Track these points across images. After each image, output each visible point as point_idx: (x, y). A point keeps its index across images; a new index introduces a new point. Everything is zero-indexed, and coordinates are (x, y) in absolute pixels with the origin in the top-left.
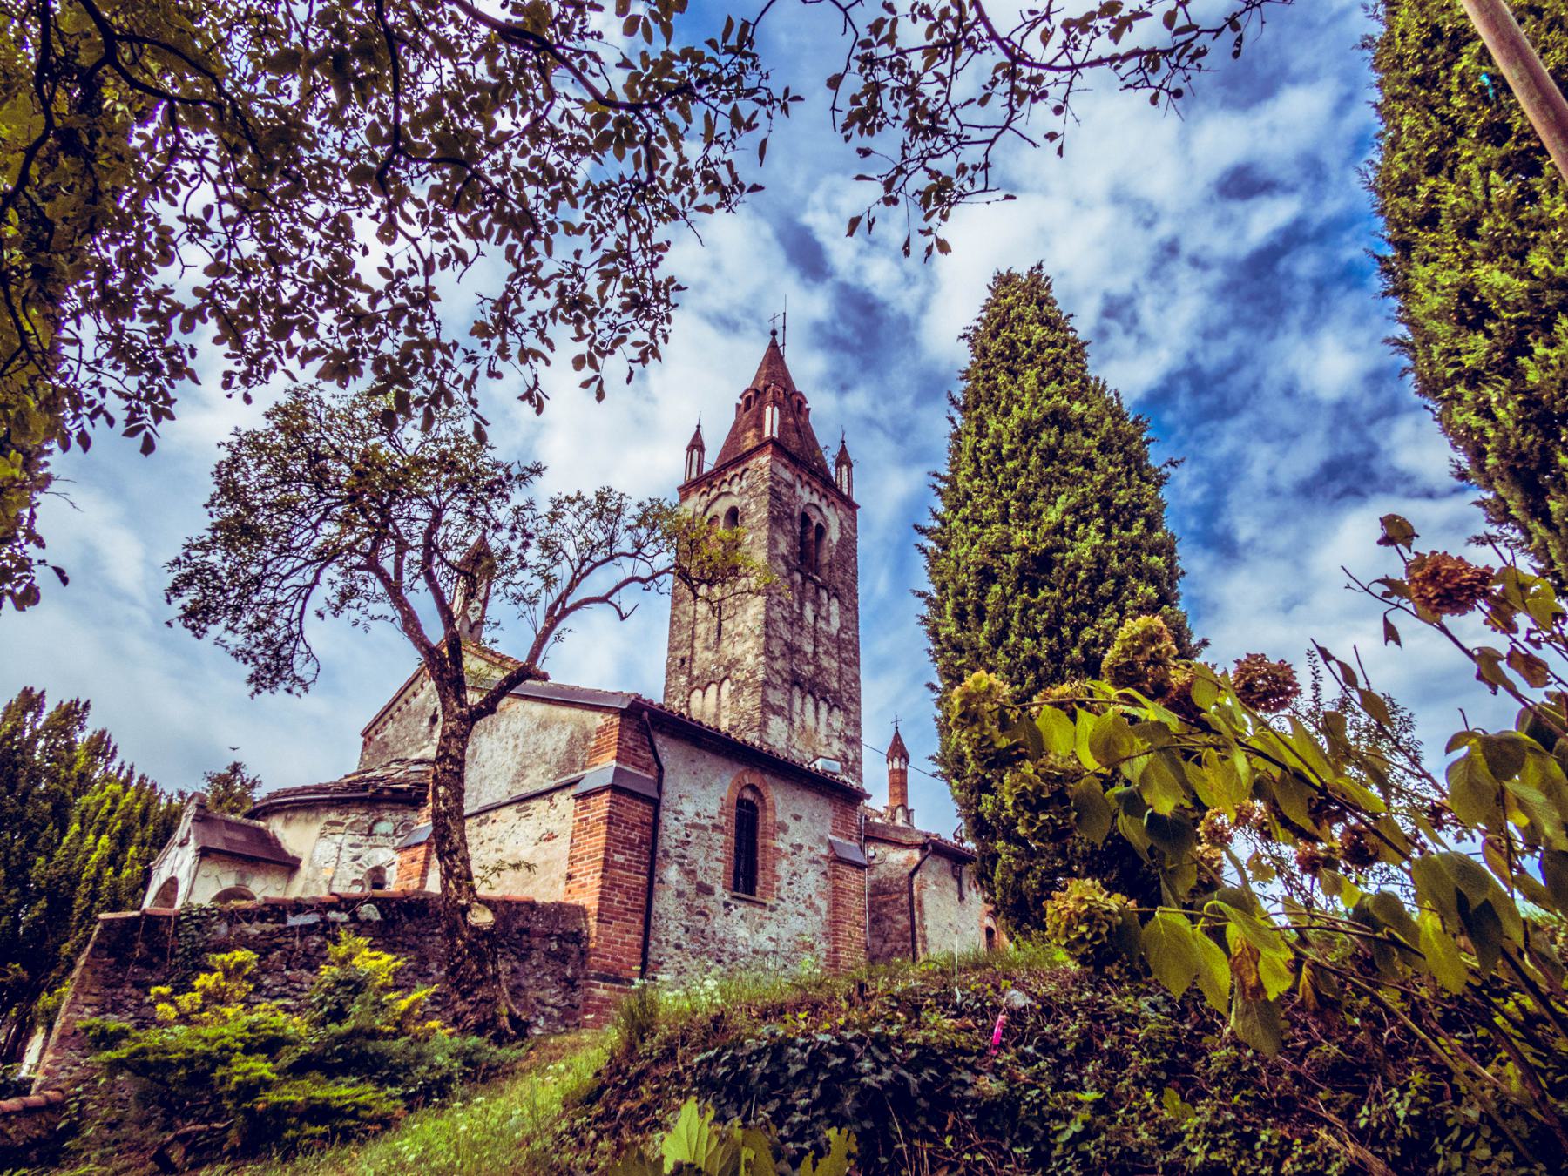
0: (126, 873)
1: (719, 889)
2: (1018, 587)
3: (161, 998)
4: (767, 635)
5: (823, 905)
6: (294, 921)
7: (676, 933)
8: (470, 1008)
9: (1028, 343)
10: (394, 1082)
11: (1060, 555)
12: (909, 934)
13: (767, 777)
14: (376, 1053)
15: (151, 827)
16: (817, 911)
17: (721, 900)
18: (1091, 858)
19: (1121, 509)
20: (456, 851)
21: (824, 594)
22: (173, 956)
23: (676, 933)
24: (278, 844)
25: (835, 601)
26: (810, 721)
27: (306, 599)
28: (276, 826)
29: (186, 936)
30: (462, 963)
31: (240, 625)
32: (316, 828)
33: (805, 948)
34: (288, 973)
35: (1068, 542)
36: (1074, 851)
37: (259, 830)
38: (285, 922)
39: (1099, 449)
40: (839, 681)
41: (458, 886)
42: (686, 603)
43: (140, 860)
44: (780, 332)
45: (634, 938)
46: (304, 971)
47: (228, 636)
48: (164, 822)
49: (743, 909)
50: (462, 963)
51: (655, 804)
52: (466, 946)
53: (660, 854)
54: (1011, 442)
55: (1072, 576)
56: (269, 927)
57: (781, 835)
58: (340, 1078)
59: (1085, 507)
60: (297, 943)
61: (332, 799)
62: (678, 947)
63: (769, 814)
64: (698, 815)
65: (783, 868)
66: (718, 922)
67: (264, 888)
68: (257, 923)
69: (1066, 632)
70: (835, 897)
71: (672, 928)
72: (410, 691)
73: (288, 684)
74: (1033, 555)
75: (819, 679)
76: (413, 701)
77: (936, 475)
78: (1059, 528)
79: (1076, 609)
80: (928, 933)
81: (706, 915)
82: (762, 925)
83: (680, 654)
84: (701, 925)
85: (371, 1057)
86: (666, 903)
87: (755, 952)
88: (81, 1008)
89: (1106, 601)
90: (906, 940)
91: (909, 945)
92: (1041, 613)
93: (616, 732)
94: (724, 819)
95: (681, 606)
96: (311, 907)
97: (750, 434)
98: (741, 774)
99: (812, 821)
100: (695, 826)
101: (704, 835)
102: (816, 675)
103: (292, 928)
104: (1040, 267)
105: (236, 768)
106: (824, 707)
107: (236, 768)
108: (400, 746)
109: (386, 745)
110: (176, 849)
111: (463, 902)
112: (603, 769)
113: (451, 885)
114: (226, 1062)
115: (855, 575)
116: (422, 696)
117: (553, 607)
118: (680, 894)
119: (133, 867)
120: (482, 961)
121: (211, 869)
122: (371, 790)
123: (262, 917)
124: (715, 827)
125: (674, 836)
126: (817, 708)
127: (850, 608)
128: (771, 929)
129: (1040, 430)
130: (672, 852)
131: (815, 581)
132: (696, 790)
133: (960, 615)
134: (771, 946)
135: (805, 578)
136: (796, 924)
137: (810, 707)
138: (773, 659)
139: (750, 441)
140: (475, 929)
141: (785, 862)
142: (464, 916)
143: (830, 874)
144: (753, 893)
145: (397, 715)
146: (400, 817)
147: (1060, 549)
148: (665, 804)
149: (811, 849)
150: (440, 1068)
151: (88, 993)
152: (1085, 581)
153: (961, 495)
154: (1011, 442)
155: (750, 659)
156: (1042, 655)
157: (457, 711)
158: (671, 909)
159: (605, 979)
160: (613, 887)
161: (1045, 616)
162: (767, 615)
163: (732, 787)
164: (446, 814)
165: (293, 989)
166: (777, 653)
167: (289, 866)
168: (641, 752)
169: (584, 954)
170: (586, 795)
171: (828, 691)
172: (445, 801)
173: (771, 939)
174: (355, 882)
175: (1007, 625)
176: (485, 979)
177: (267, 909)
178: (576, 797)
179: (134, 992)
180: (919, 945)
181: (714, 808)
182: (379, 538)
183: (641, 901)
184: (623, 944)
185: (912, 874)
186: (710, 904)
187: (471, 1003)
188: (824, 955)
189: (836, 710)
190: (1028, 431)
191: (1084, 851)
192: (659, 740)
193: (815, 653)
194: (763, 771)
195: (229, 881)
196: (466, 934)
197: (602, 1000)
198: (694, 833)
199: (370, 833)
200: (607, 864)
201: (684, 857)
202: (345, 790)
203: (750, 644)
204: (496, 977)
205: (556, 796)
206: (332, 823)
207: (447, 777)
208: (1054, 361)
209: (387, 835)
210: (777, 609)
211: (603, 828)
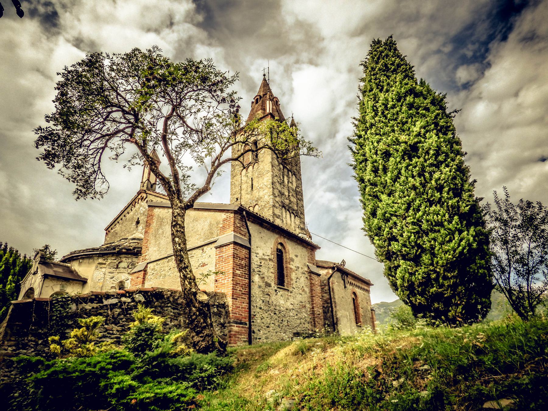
0: (8, 287)
1: (273, 284)
2: (403, 158)
3: (54, 341)
4: (273, 187)
5: (307, 290)
6: (106, 302)
7: (259, 303)
8: (201, 339)
9: (392, 64)
10: (185, 379)
11: (421, 145)
12: (329, 301)
13: (286, 240)
14: (173, 365)
15: (18, 268)
16: (306, 293)
17: (274, 289)
18: (446, 265)
19: (442, 127)
20: (187, 267)
21: (290, 173)
22: (51, 320)
23: (259, 303)
24: (77, 273)
25: (294, 176)
26: (289, 222)
27: (101, 154)
28: (75, 266)
29: (57, 311)
30: (196, 318)
31: (70, 165)
32: (93, 267)
33: (303, 307)
34: (106, 326)
35: (423, 140)
36: (437, 263)
37: (68, 267)
38: (102, 303)
39: (431, 103)
40: (297, 206)
41: (190, 283)
42: (237, 177)
43: (14, 282)
44: (267, 75)
45: (245, 305)
46: (113, 325)
47: (64, 169)
48: (23, 265)
49: (281, 292)
50: (196, 318)
51: (249, 249)
52: (197, 311)
53: (252, 270)
54: (393, 101)
55: (427, 153)
56: (95, 305)
57: (292, 263)
58: (160, 380)
59: (428, 126)
60: (109, 312)
61: (100, 254)
62: (260, 308)
63: (287, 254)
64: (264, 255)
65: (293, 276)
66: (273, 297)
67: (72, 291)
68: (89, 304)
69: (427, 175)
70: (311, 287)
71: (258, 301)
72: (126, 212)
73: (92, 195)
74: (410, 145)
75: (291, 205)
76: (128, 216)
77: (354, 118)
78: (419, 134)
79: (431, 165)
80: (336, 300)
81: (269, 295)
82: (288, 299)
83: (236, 196)
84: (268, 299)
85: (171, 367)
86: (255, 290)
87: (287, 309)
88: (6, 347)
89: (442, 163)
90: (328, 303)
91: (329, 305)
92: (415, 167)
93: (232, 220)
94: (273, 256)
95: (235, 178)
96: (113, 296)
97: (260, 112)
98: (277, 238)
99: (301, 257)
100: (263, 259)
101: (266, 263)
102: (290, 204)
103: (106, 306)
104: (391, 37)
105: (47, 247)
106: (293, 216)
107: (47, 247)
108: (123, 234)
109: (117, 233)
110: (31, 276)
111: (194, 290)
112: (229, 236)
113: (187, 283)
114: (105, 376)
115: (300, 167)
116: (131, 213)
117: (214, 163)
118: (260, 287)
119: (11, 284)
120: (205, 317)
121: (48, 283)
122: (117, 250)
123: (92, 301)
124: (270, 260)
125: (256, 263)
126: (291, 216)
127: (299, 179)
128: (291, 300)
129: (406, 96)
130: (256, 270)
131: (287, 169)
132: (262, 244)
133: (375, 171)
134: (291, 307)
135: (284, 167)
136: (299, 298)
137: (288, 216)
138: (276, 197)
139: (260, 113)
140: (201, 302)
141: (294, 273)
142: (195, 296)
143: (309, 278)
144: (284, 286)
145: (120, 221)
146: (130, 261)
147: (420, 142)
148: (252, 250)
149: (302, 268)
150: (206, 370)
151: (10, 340)
152: (434, 154)
153: (368, 125)
154: (393, 101)
155: (266, 197)
156: (418, 184)
157: (179, 205)
158: (257, 293)
159: (236, 323)
160: (237, 284)
161: (417, 169)
162: (273, 180)
163: (275, 244)
164: (181, 251)
165: (109, 333)
166: (277, 195)
167: (84, 282)
168: (242, 229)
169: (227, 313)
170: (221, 246)
171: (294, 210)
172: (179, 244)
173: (292, 304)
174: (112, 287)
175: (400, 173)
176: (207, 325)
177: (93, 297)
178: (216, 248)
179: (33, 338)
180: (333, 305)
181: (269, 252)
182: (134, 127)
183: (247, 290)
184: (242, 308)
185: (329, 279)
186: (270, 291)
187: (201, 337)
188: (309, 309)
189: (297, 217)
190: (399, 98)
191: (443, 263)
192: (249, 223)
193: (289, 196)
194: (285, 237)
195: (57, 289)
196: (197, 305)
197: (236, 332)
198: (263, 262)
199: (117, 267)
200: (234, 275)
201: (260, 272)
202: (105, 250)
203: (266, 191)
204: (211, 325)
205: (205, 248)
206: (100, 264)
207: (179, 234)
208: (405, 71)
209: (125, 268)
210: (276, 178)
211: (231, 259)
